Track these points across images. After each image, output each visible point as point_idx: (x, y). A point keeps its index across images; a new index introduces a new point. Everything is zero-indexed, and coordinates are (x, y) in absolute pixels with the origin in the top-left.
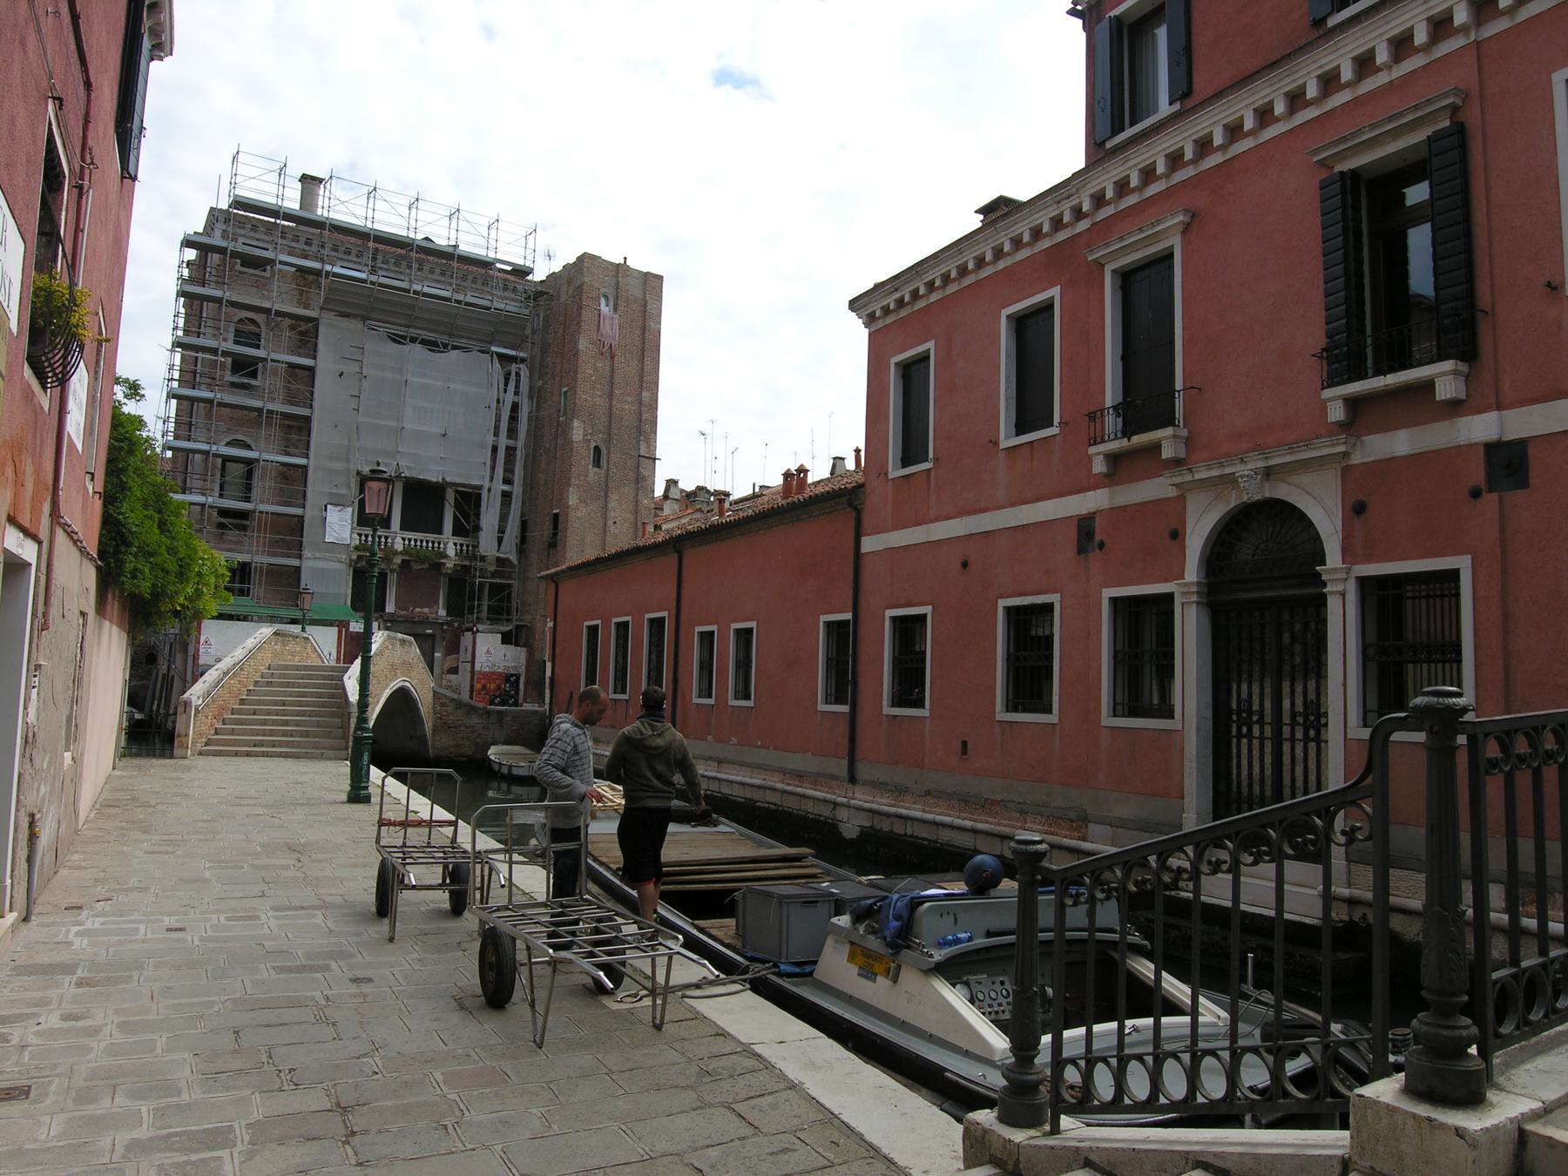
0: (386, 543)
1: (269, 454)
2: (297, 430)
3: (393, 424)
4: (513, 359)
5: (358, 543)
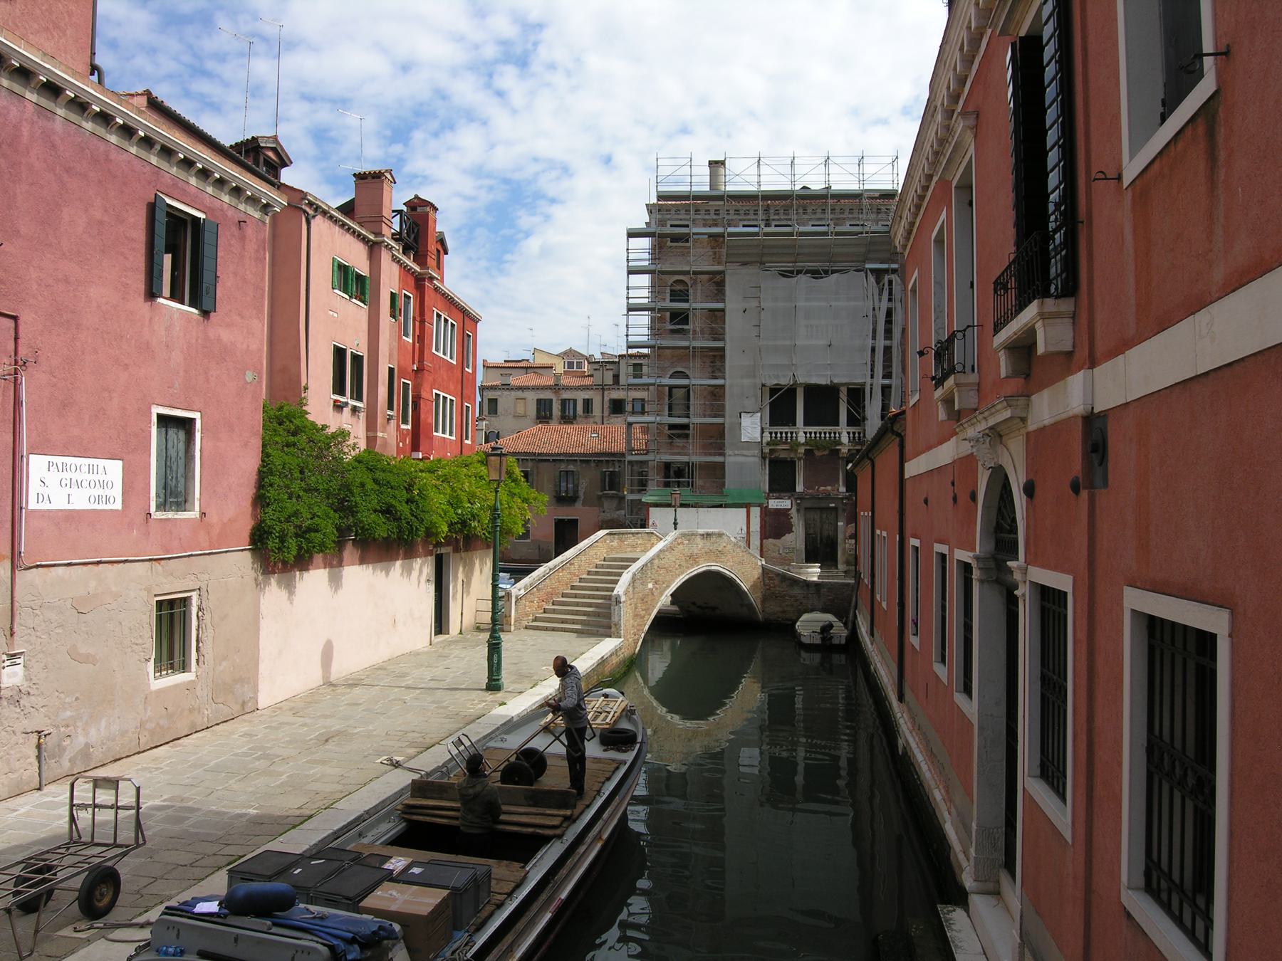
0: (792, 437)
1: (699, 380)
2: (716, 358)
3: (788, 342)
4: (886, 271)
5: (769, 439)
